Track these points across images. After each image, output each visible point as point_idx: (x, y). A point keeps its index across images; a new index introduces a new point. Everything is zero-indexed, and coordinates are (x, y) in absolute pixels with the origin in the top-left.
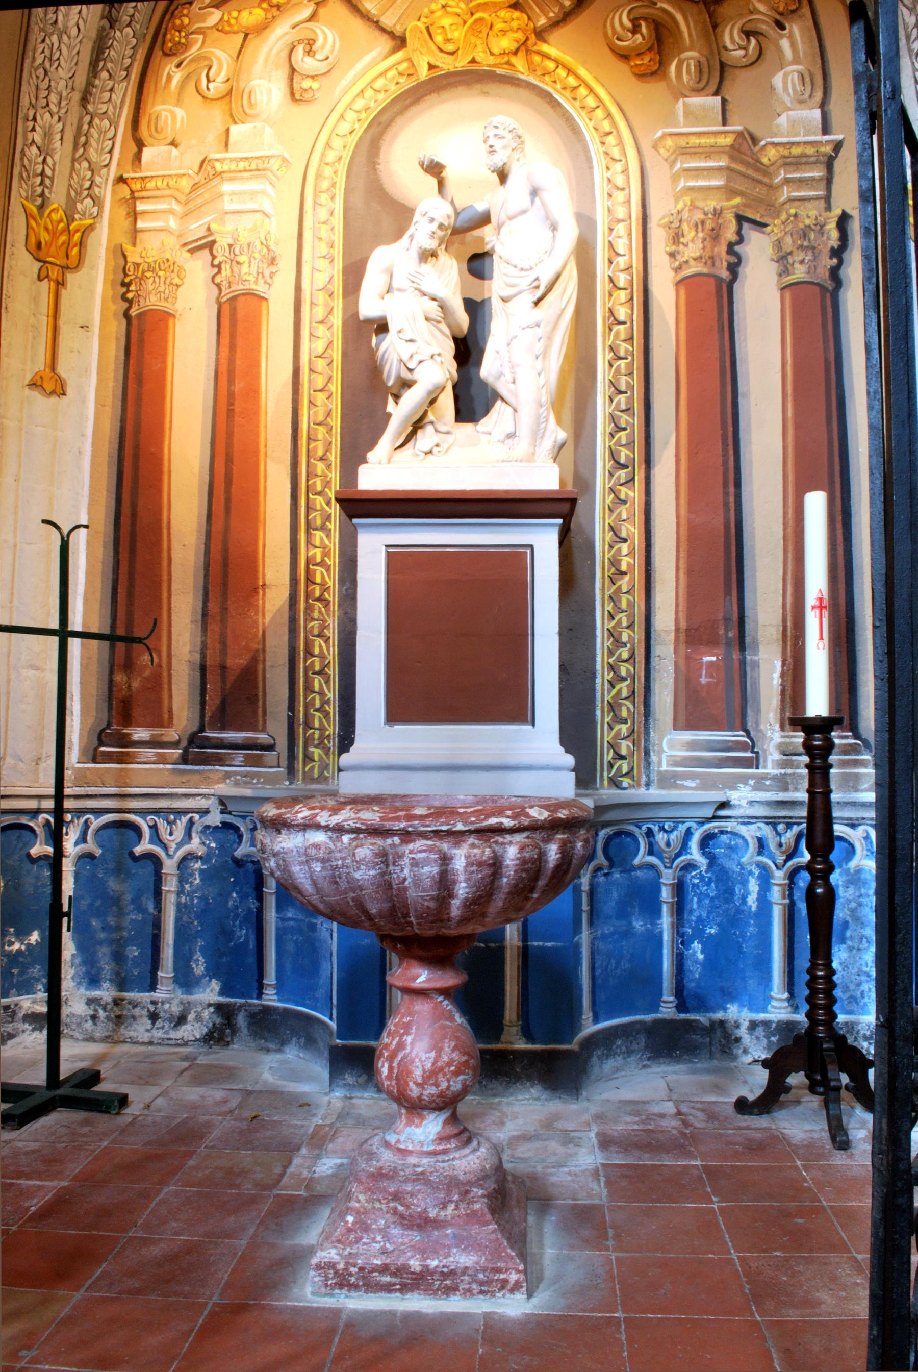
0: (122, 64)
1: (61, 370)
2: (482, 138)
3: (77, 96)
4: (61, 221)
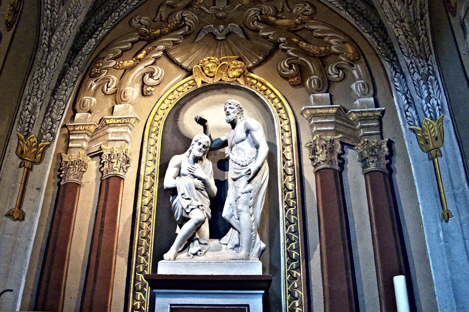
0: (72, 80)
1: (24, 209)
2: (224, 109)
3: (50, 92)
4: (35, 142)
